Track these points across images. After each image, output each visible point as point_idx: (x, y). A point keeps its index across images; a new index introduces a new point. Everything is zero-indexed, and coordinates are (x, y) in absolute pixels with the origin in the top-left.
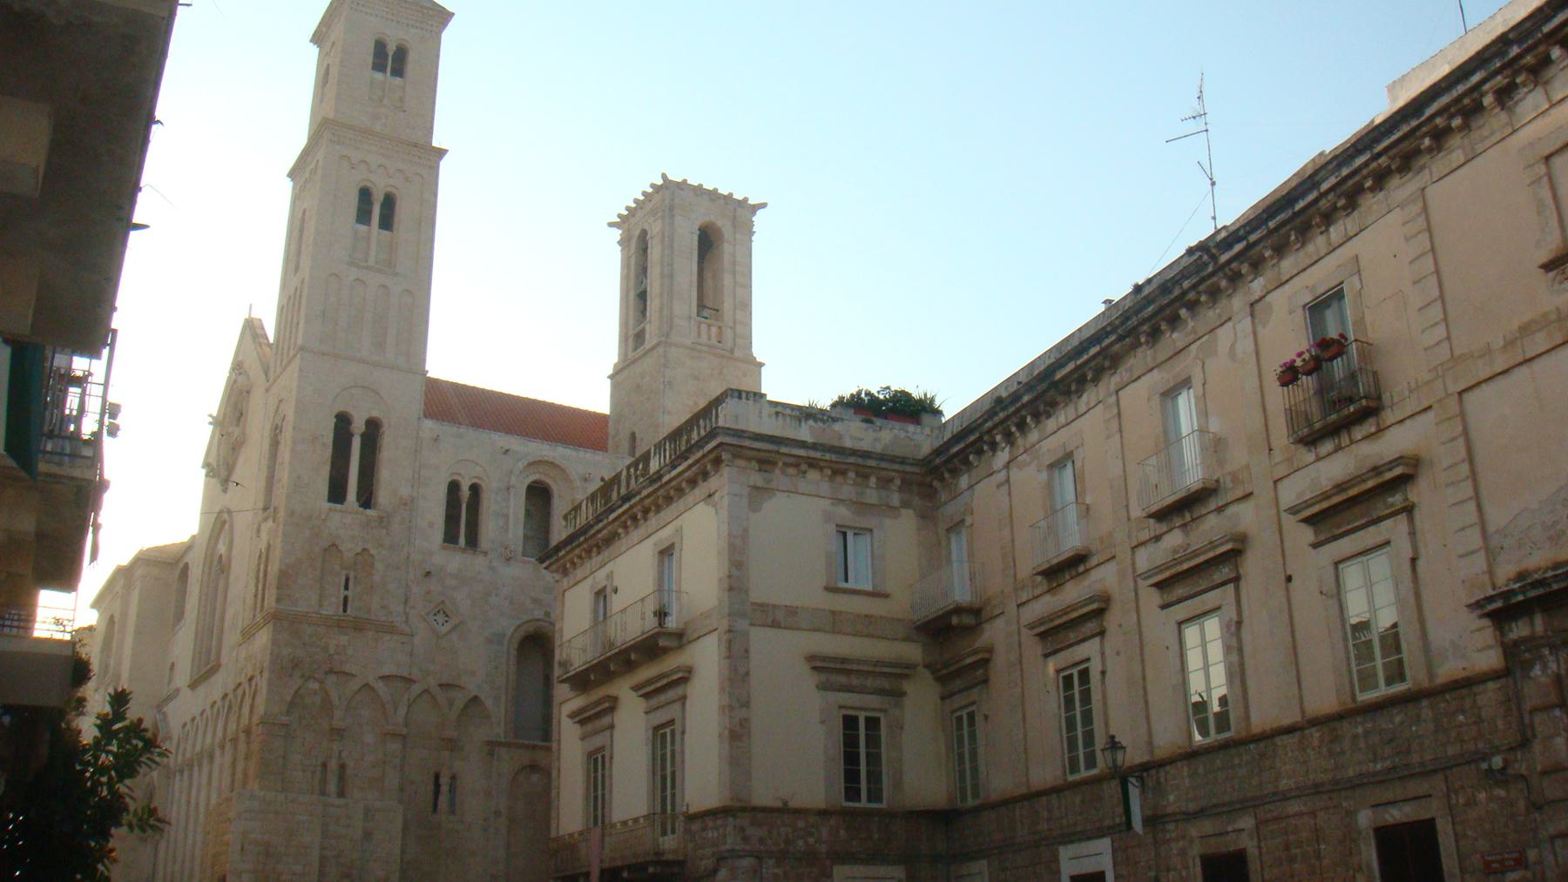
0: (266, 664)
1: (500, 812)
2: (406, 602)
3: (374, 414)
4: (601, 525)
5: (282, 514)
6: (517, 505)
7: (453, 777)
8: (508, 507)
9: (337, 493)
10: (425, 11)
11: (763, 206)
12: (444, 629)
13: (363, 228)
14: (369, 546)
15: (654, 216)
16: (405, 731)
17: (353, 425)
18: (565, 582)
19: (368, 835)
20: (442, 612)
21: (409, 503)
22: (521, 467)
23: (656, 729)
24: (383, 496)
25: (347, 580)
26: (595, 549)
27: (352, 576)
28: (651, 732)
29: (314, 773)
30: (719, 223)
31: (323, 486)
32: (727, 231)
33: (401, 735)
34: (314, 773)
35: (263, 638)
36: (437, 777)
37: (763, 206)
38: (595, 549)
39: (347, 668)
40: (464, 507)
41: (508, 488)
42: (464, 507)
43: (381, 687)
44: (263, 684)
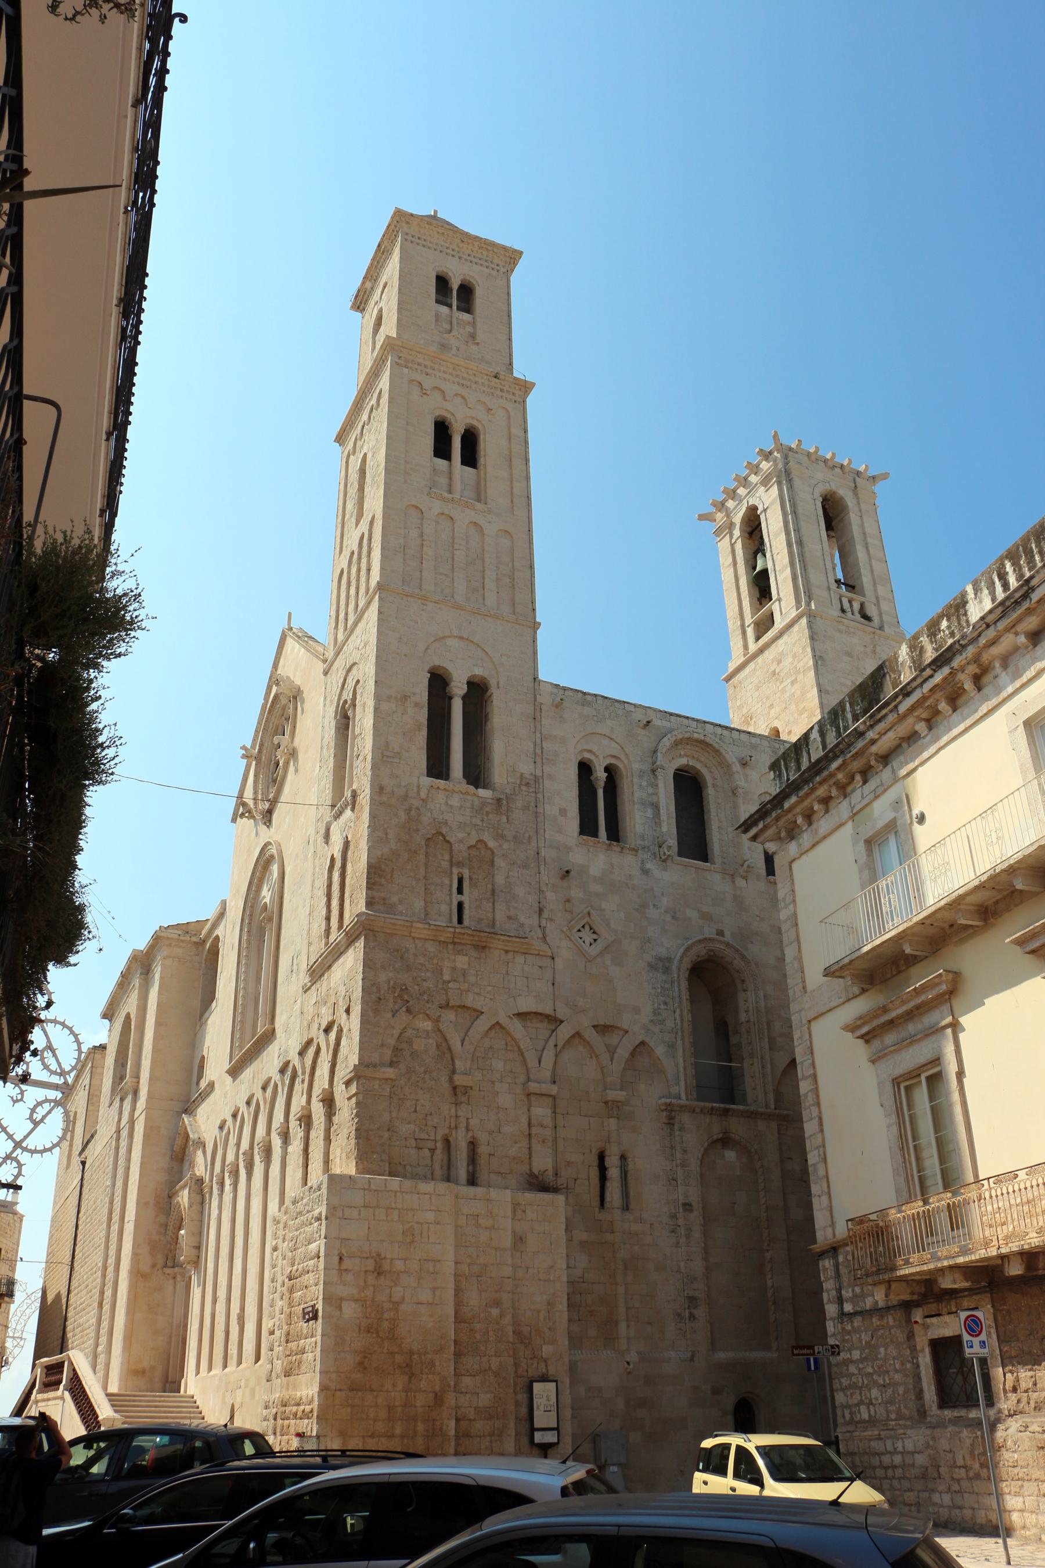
0: (358, 993)
1: (690, 1205)
2: (541, 911)
3: (478, 671)
4: (880, 727)
5: (365, 799)
6: (666, 793)
7: (623, 1158)
8: (656, 794)
9: (438, 767)
10: (490, 248)
11: (885, 476)
12: (593, 951)
13: (441, 463)
14: (486, 837)
15: (765, 486)
16: (554, 1089)
17: (453, 684)
18: (793, 848)
19: (519, 1240)
20: (587, 928)
21: (533, 784)
22: (668, 744)
23: (896, 1082)
24: (499, 773)
25: (460, 881)
26: (858, 777)
27: (466, 876)
28: (888, 1087)
29: (433, 1151)
30: (841, 492)
31: (418, 755)
32: (850, 501)
33: (550, 1096)
34: (433, 1151)
35: (352, 961)
36: (601, 1157)
37: (885, 476)
38: (858, 777)
39: (469, 1000)
40: (600, 793)
41: (653, 771)
42: (600, 793)
43: (517, 1028)
44: (353, 1025)
